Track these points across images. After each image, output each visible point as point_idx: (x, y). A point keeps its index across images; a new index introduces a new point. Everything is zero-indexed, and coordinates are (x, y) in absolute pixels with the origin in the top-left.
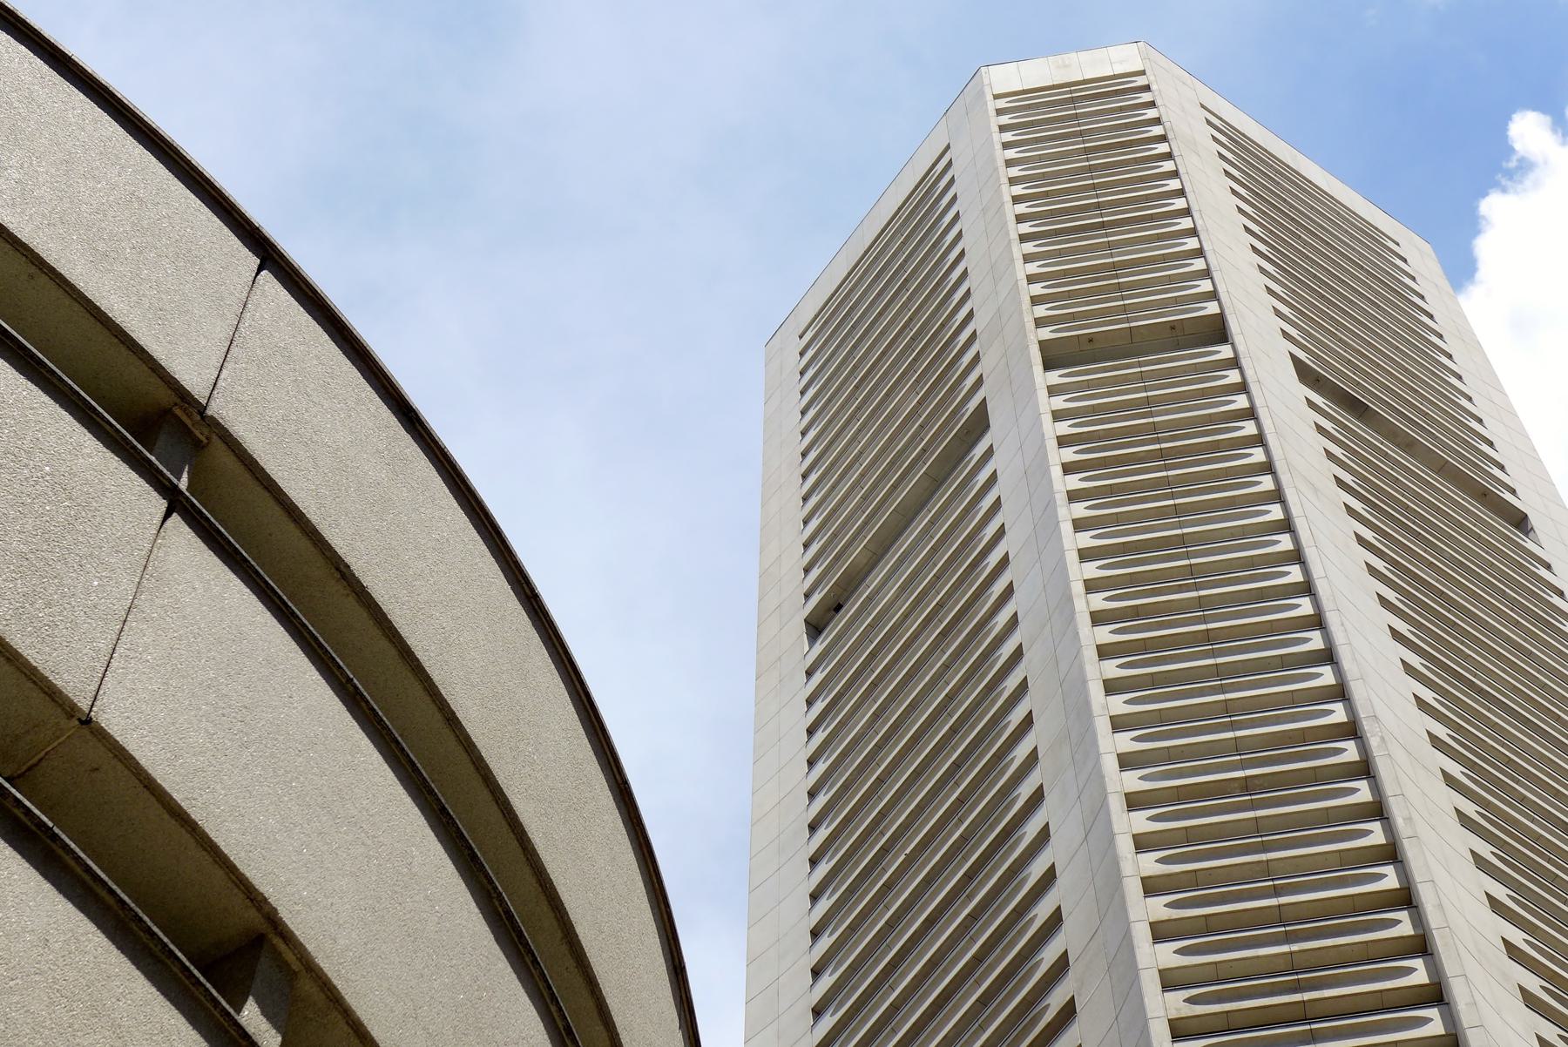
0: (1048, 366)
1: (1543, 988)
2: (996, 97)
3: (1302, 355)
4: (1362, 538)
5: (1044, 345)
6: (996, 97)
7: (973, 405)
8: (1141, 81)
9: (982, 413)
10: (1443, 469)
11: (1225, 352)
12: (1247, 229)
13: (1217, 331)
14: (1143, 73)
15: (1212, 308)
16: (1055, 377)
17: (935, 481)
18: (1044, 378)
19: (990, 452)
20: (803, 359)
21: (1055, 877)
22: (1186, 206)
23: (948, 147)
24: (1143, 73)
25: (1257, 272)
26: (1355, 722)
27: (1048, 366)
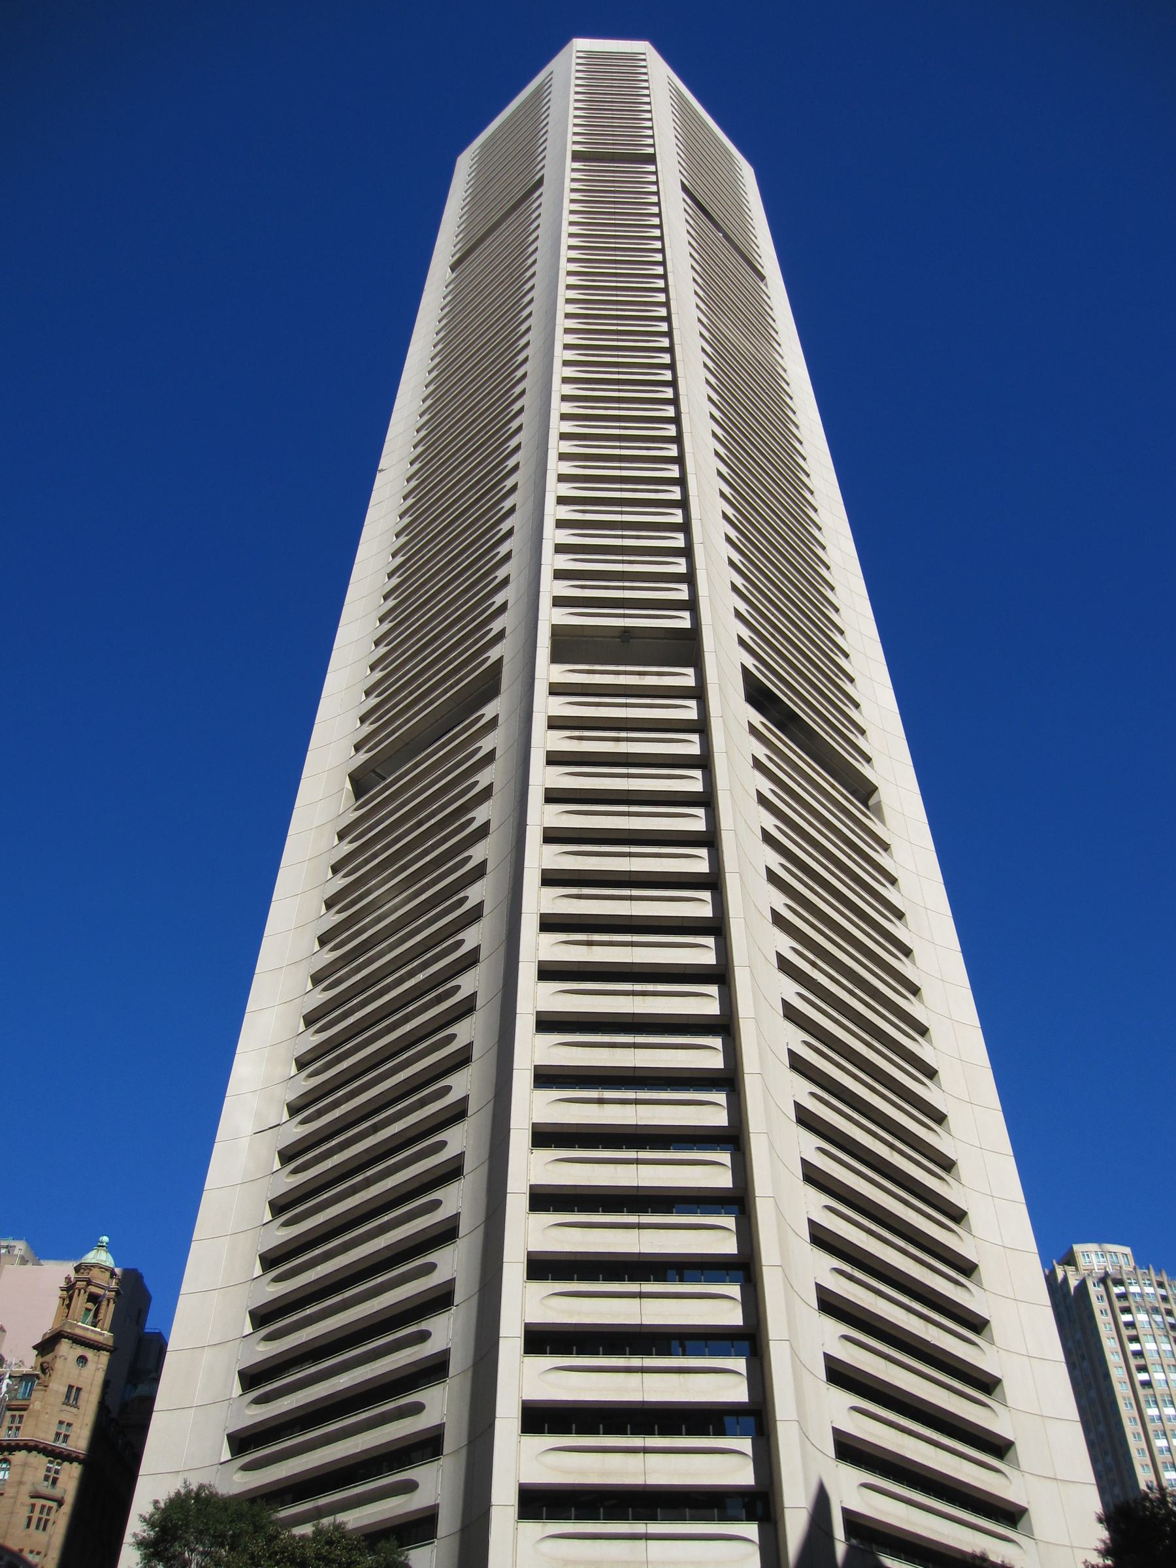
0: (557, 656)
1: (740, 561)
2: (578, 51)
3: (686, 183)
4: (718, 452)
5: (558, 632)
6: (578, 51)
7: (537, 177)
8: (643, 57)
9: (542, 178)
10: (737, 248)
11: (652, 168)
12: (696, 293)
13: (651, 159)
14: (644, 54)
15: (650, 150)
16: (577, 165)
17: (514, 208)
18: (569, 164)
19: (541, 195)
20: (425, 404)
21: (522, 428)
22: (653, 152)
23: (552, 72)
24: (644, 54)
25: (674, 138)
26: (726, 965)
27: (557, 656)
